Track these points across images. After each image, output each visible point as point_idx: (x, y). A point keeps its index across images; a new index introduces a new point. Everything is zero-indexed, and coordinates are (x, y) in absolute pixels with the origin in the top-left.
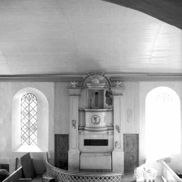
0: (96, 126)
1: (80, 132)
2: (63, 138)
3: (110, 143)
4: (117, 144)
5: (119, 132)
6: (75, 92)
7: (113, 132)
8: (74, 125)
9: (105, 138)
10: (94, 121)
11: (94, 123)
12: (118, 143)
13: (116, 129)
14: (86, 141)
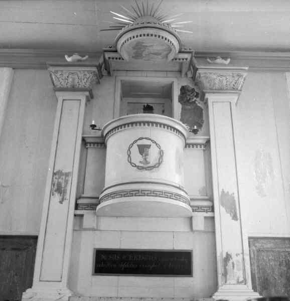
0: (146, 175)
1: (82, 216)
2: (14, 253)
3: (199, 263)
4: (230, 264)
5: (235, 217)
6: (74, 79)
7: (213, 218)
8: (59, 189)
9: (180, 245)
10: (137, 158)
11: (138, 167)
12: (235, 259)
13: (222, 204)
14: (103, 257)
